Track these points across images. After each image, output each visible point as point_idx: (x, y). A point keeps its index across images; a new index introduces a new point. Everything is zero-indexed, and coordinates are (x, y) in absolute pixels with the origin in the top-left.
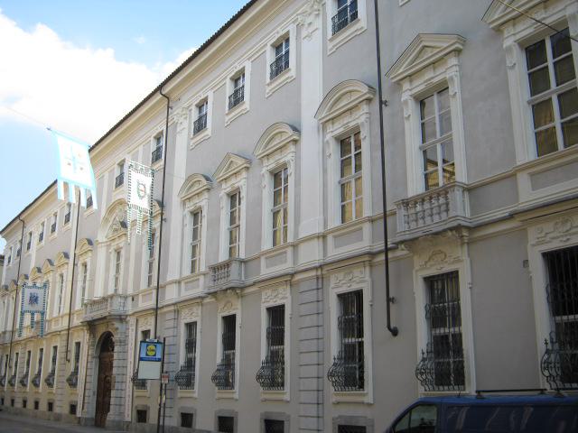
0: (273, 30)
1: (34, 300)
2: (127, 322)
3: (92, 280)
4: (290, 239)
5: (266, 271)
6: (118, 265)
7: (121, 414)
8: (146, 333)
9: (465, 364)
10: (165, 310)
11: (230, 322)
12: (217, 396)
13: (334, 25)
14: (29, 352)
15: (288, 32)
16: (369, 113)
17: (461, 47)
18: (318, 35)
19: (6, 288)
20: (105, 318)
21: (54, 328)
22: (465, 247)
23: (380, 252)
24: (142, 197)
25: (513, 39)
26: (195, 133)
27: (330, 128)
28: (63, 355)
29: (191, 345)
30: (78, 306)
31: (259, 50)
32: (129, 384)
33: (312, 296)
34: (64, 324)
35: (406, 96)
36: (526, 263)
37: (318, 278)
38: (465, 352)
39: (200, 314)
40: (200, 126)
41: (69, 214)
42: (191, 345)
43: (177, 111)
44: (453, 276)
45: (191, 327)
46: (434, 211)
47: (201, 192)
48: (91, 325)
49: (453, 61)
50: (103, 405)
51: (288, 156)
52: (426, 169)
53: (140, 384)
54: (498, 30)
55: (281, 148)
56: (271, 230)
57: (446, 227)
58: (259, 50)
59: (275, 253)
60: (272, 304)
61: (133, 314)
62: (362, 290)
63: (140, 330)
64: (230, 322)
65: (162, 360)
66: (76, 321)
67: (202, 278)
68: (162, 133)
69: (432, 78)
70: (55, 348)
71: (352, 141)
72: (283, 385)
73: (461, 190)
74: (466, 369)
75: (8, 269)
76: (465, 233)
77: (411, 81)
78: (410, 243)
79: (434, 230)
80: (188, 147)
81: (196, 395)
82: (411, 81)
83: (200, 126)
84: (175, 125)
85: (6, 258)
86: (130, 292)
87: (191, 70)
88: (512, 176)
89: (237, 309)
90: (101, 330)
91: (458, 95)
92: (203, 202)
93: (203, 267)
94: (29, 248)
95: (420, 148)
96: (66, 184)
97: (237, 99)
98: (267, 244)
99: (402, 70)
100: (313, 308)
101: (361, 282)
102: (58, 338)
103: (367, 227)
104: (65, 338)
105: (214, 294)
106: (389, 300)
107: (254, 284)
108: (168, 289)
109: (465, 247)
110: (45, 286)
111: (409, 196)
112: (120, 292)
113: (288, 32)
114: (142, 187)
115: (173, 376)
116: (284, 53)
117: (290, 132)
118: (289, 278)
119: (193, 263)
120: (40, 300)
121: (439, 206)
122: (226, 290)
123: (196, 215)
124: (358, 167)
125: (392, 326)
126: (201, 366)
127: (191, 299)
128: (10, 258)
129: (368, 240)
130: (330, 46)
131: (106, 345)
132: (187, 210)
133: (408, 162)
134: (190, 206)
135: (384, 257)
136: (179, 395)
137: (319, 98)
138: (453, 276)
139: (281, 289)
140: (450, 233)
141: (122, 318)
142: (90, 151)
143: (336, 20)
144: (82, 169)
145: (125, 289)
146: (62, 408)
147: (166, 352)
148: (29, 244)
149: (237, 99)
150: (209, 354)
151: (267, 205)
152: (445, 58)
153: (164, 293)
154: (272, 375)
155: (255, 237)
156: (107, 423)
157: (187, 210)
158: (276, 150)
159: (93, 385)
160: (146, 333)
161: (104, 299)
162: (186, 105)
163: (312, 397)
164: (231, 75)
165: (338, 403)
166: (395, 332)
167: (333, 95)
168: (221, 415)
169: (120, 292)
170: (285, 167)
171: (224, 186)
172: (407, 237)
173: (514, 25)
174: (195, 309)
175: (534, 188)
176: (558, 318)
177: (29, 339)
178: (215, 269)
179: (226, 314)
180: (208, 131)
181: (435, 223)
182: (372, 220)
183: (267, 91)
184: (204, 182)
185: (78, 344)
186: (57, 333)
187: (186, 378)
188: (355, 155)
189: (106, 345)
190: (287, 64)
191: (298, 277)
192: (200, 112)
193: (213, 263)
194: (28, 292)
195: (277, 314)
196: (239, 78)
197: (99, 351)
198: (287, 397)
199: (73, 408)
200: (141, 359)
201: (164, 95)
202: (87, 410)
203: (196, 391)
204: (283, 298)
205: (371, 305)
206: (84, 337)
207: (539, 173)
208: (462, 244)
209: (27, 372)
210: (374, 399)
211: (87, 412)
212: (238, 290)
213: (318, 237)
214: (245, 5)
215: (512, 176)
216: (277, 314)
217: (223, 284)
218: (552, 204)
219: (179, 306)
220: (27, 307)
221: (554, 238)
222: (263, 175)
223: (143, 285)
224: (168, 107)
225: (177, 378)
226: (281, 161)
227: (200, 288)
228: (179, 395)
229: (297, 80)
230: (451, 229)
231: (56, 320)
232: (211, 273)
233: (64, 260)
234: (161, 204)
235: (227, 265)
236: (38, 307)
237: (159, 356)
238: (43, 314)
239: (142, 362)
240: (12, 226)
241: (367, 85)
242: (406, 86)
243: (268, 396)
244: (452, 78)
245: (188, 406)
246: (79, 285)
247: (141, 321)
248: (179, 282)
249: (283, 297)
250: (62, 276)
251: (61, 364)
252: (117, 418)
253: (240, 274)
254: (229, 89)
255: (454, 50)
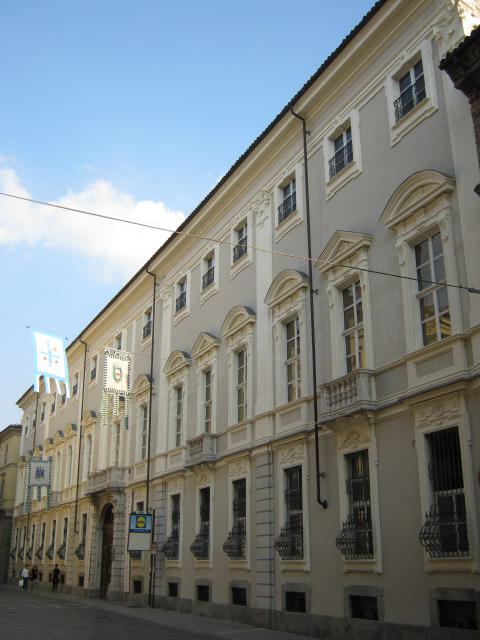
0: (398, 54)
1: (40, 473)
2: (125, 494)
3: (96, 453)
4: (456, 329)
5: (232, 445)
6: (118, 437)
7: (120, 585)
8: (140, 505)
9: (468, 529)
10: (155, 482)
11: (205, 493)
12: (196, 566)
13: (280, 215)
14: (44, 524)
15: (420, 52)
16: (217, 357)
17: (368, 243)
18: (268, 222)
19: (24, 459)
20: (104, 490)
21: (65, 500)
22: (373, 428)
23: (311, 431)
24: (117, 381)
25: (403, 239)
26: (280, 220)
27: (401, 231)
28: (73, 527)
29: (176, 516)
30: (84, 479)
31: (376, 86)
32: (127, 556)
33: (265, 471)
34: (72, 496)
35: (330, 287)
36: (414, 442)
37: (269, 454)
38: (467, 516)
39: (305, 455)
40: (181, 303)
41: (95, 370)
42: (176, 516)
43: (162, 289)
44: (364, 453)
45: (176, 498)
46: (333, 400)
47: (295, 293)
48: (94, 497)
49: (363, 256)
50: (105, 578)
51: (246, 338)
52: (423, 318)
53: (136, 555)
54: (394, 229)
55: (291, 296)
56: (141, 448)
57: (353, 410)
58: (376, 86)
59: (292, 408)
60: (236, 478)
61: (130, 485)
62: (457, 428)
63: (135, 503)
64: (205, 493)
65: (152, 532)
66: (82, 494)
67: (184, 452)
68: (150, 308)
69: (424, 222)
70: (66, 519)
71: (354, 288)
72: (371, 552)
73: (366, 378)
74: (469, 533)
75: (26, 440)
76: (210, 465)
77: (334, 272)
78: (330, 423)
79: (348, 412)
80: (273, 242)
81: (179, 565)
82: (334, 272)
83: (181, 303)
84: (162, 301)
85: (24, 428)
86: (127, 464)
87: (331, 75)
88: (402, 364)
89: (210, 482)
90: (104, 502)
91: (450, 240)
92: (183, 378)
93: (183, 443)
94: (43, 419)
95: (343, 335)
96: (52, 381)
97: (209, 279)
98: (233, 421)
99: (328, 262)
100: (264, 482)
101: (454, 417)
102: (68, 510)
103: (304, 407)
104: (74, 509)
105: (191, 468)
106: (319, 475)
107: (401, 401)
108: (158, 460)
109: (373, 428)
110: (51, 459)
111: (334, 378)
112: (120, 465)
113: (420, 52)
114: (118, 371)
115: (161, 546)
116: (345, 144)
117: (247, 315)
118: (247, 454)
119: (290, 388)
120: (46, 474)
121: (335, 396)
122: (200, 464)
123: (179, 389)
124: (360, 318)
125: (322, 500)
126: (214, 531)
127: (176, 472)
128: (53, 406)
129: (303, 421)
130: (277, 234)
131: (107, 516)
132: (276, 320)
133: (332, 345)
134: (174, 382)
135: (312, 436)
136: (167, 565)
137: (269, 281)
138: (364, 453)
139: (449, 406)
140: (356, 416)
141: (120, 491)
142: (67, 350)
143: (334, 164)
144: (56, 362)
145: (123, 462)
146: (265, 598)
147: (156, 523)
148: (43, 415)
149: (209, 279)
150: (268, 513)
151: (233, 384)
152: (415, 215)
153: (154, 465)
154: (235, 547)
155: (223, 415)
156: (109, 595)
157: (276, 320)
158: (287, 298)
159: (98, 558)
160: (140, 505)
161: (105, 472)
162: (169, 283)
163: (265, 566)
164: (203, 257)
165: (349, 572)
166: (325, 505)
167: (279, 282)
168: (200, 584)
169: (120, 465)
170: (434, 232)
171: (200, 364)
172: (329, 418)
173: (405, 226)
174: (297, 449)
175: (419, 374)
176: (437, 493)
177: (43, 511)
178: (192, 443)
179: (203, 487)
180: (187, 309)
181: (346, 407)
182: (307, 401)
183: (327, 193)
184: (185, 358)
185: (85, 516)
186: (66, 505)
187: (171, 549)
188: (435, 262)
189: (107, 516)
190: (351, 157)
191: (255, 452)
192: (285, 195)
193: (192, 437)
194: (34, 466)
195: (240, 485)
196: (242, 230)
197: (103, 522)
198: (307, 567)
199: (81, 580)
200: (131, 531)
201: (296, 115)
202: (92, 582)
203: (180, 562)
204: (364, 442)
205: (470, 446)
206: (89, 509)
207: (236, 432)
208: (370, 425)
209: (43, 545)
210: (383, 568)
211: (92, 584)
212: (209, 464)
213: (269, 415)
214: (369, 10)
215: (402, 364)
216: (240, 485)
217: (198, 458)
218: (435, 389)
219: (166, 478)
220: (34, 481)
221: (432, 422)
222: (228, 355)
223: (138, 458)
224: (305, 132)
225: (165, 549)
226: (292, 310)
227: (181, 462)
228: (167, 565)
229: (253, 264)
230: (358, 412)
231: (67, 491)
232: (189, 448)
233: (72, 432)
234: (151, 379)
235: (200, 440)
236: (44, 480)
237: (149, 527)
238: (49, 487)
239: (131, 534)
240: (27, 398)
241: (444, 175)
242: (331, 277)
243: (351, 567)
244: (442, 222)
245: (173, 575)
246: (86, 457)
247: (171, 485)
248: (166, 456)
249: (243, 471)
250: (71, 447)
251: (70, 536)
252: (117, 589)
253: (212, 449)
254: (234, 241)
255: (445, 192)
